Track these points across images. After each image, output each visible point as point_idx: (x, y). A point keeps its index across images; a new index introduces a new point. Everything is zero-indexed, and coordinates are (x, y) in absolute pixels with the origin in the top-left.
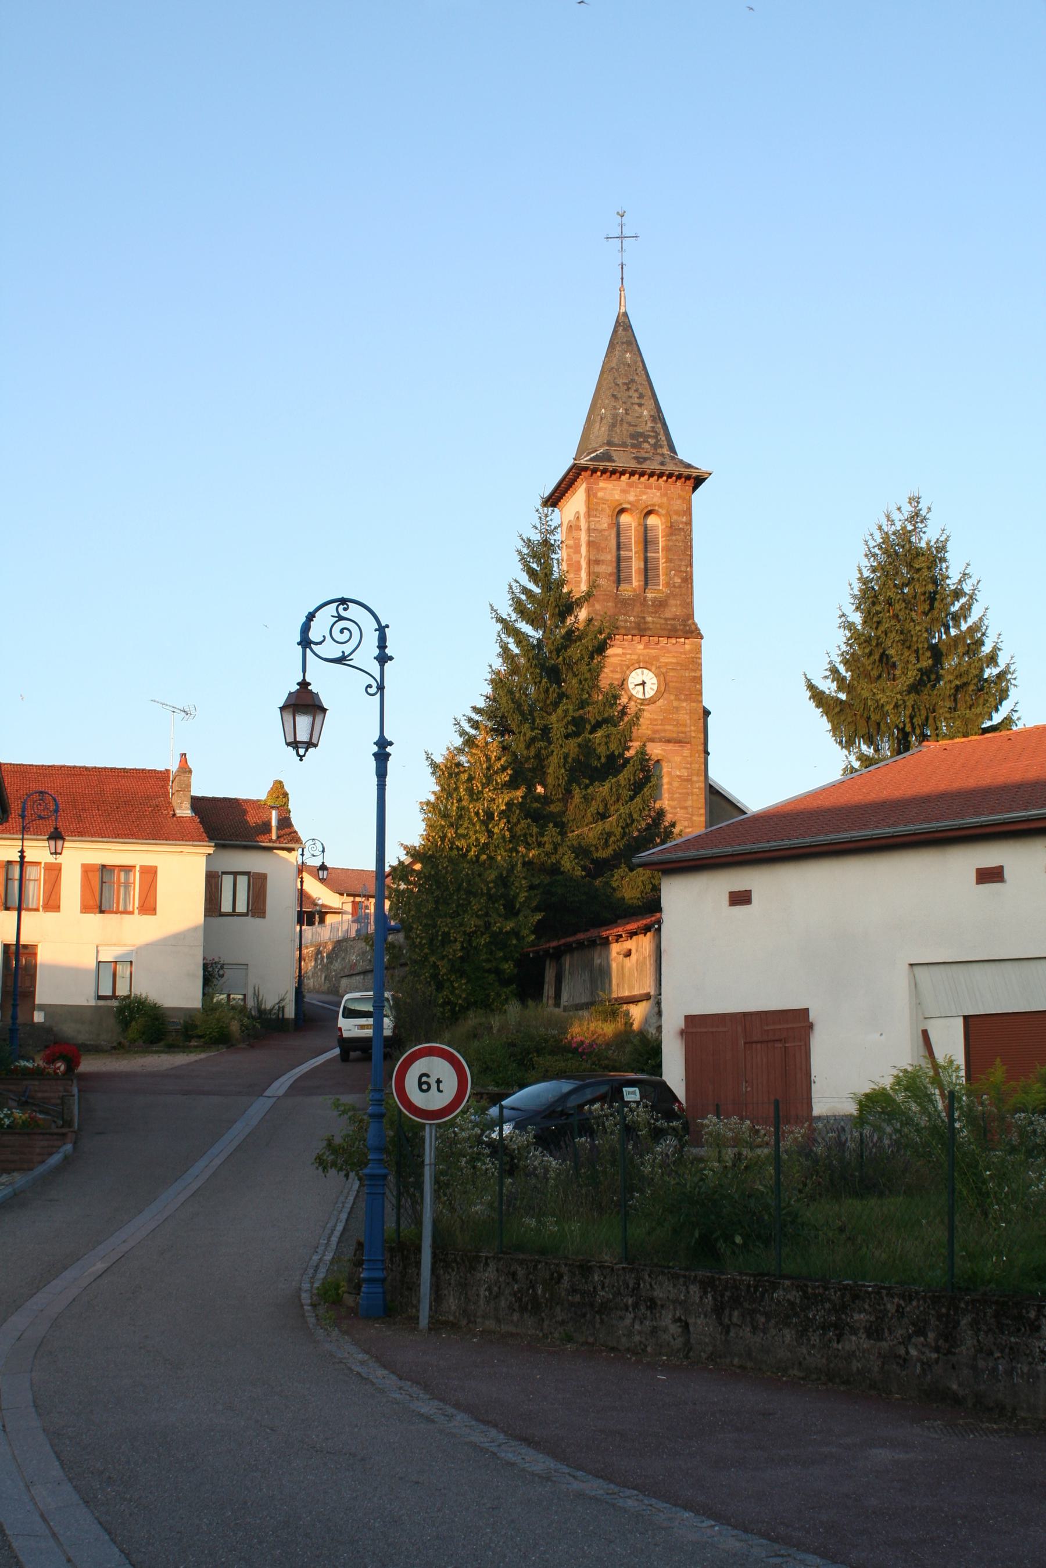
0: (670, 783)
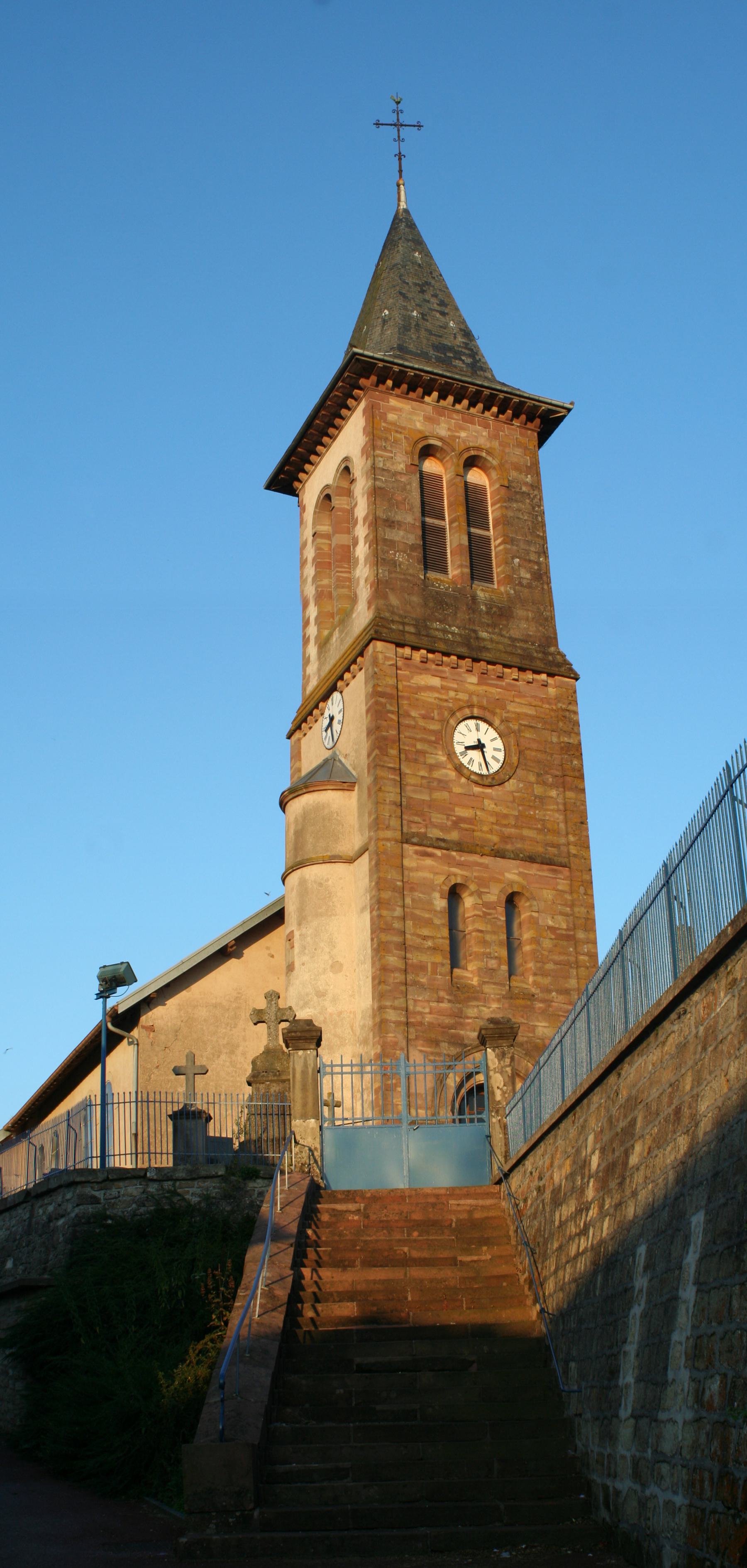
0: (535, 941)
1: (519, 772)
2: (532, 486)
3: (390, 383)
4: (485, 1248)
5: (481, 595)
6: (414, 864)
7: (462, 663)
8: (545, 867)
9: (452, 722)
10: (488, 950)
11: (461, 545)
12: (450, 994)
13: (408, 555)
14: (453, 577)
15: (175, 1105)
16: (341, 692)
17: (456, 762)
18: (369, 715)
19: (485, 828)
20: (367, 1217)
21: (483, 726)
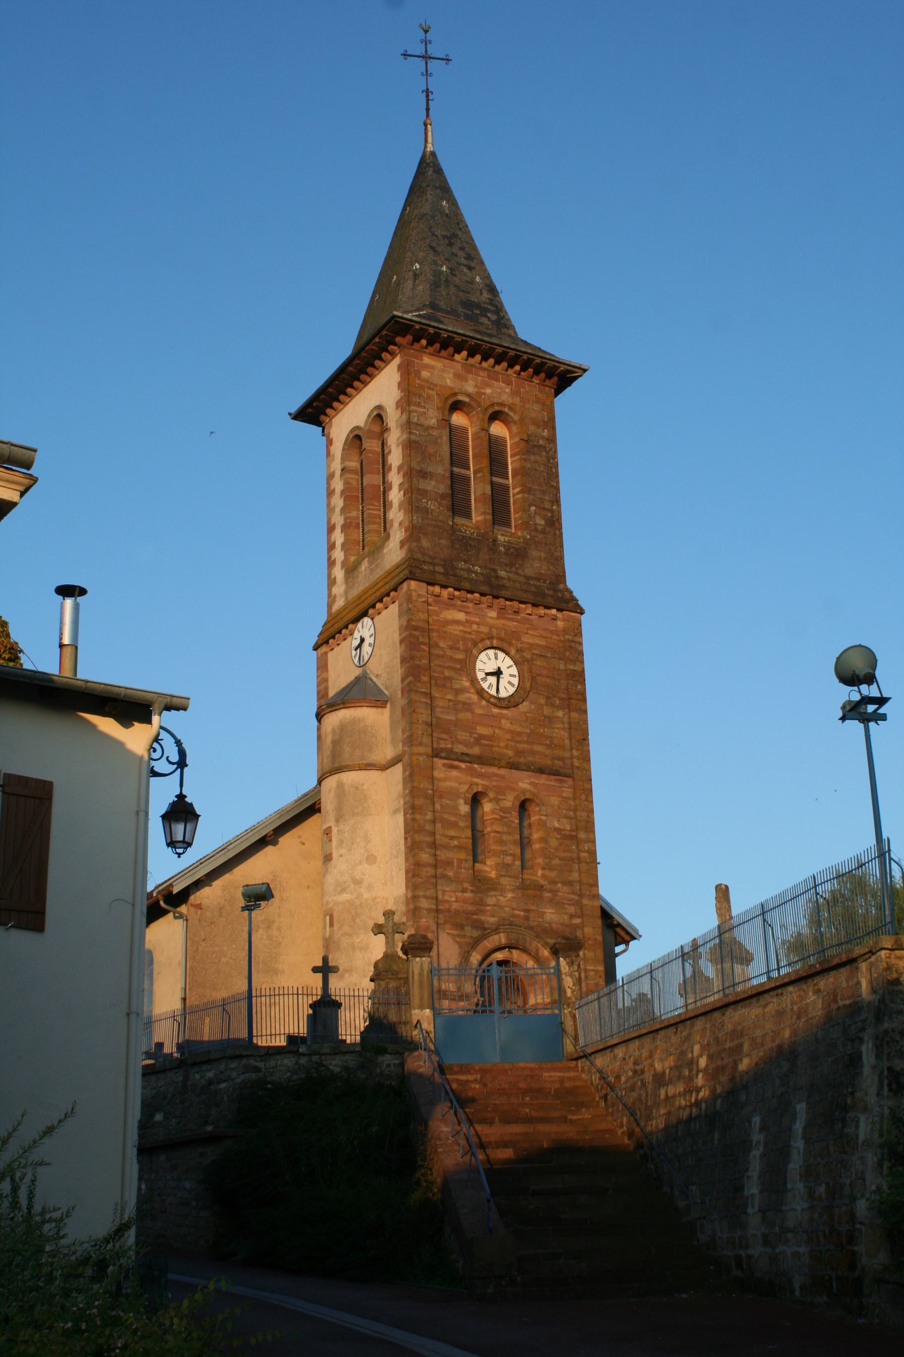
0: (543, 840)
1: (531, 695)
2: (548, 440)
3: (424, 342)
4: (584, 1110)
5: (501, 538)
6: (442, 775)
7: (484, 599)
8: (552, 777)
9: (475, 652)
10: (504, 848)
11: (484, 494)
12: (473, 885)
13: (439, 503)
14: (477, 522)
15: (310, 997)
16: (372, 619)
17: (478, 686)
18: (403, 645)
19: (502, 744)
20: (485, 1085)
21: (501, 655)
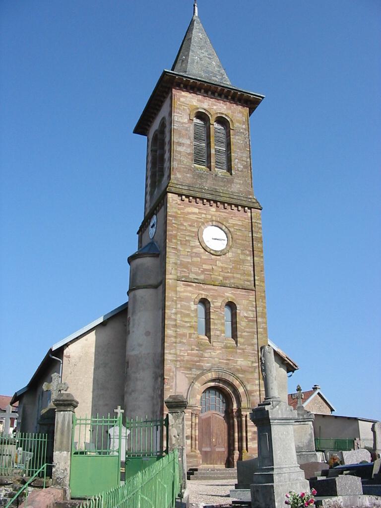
10: (216, 327)
